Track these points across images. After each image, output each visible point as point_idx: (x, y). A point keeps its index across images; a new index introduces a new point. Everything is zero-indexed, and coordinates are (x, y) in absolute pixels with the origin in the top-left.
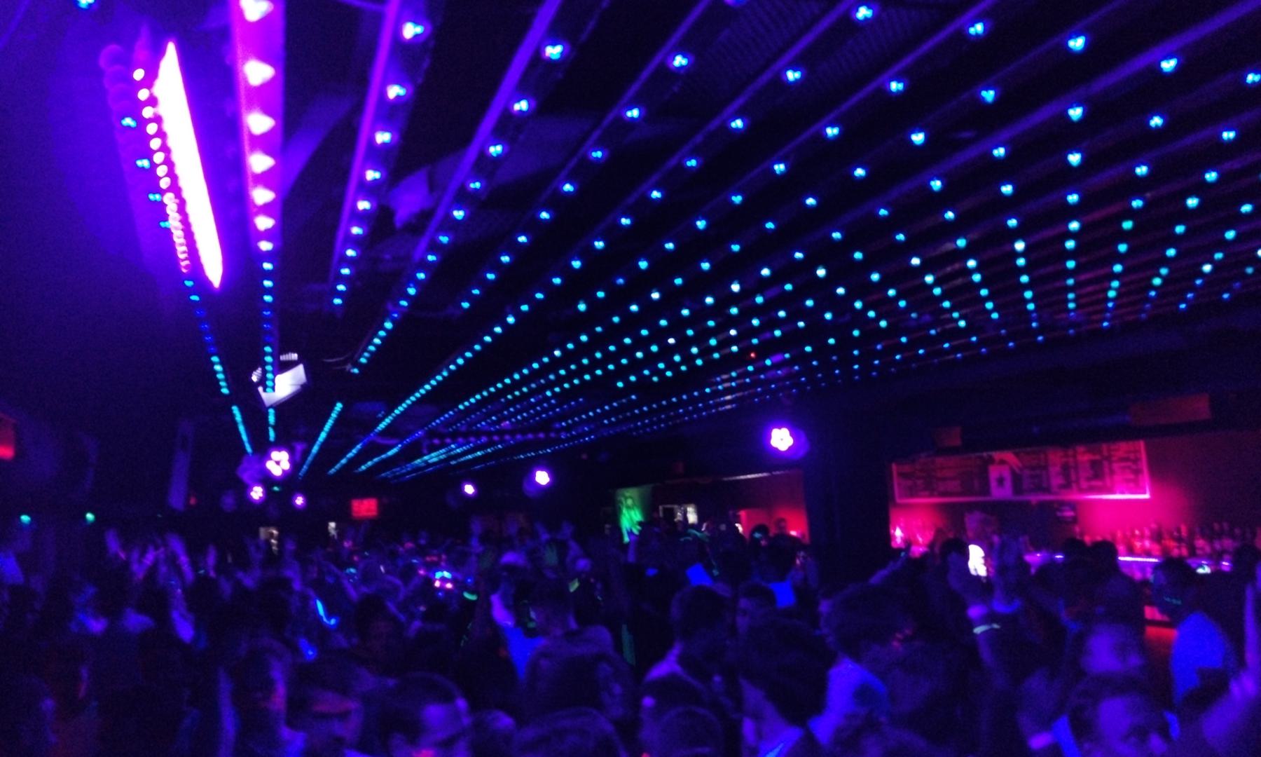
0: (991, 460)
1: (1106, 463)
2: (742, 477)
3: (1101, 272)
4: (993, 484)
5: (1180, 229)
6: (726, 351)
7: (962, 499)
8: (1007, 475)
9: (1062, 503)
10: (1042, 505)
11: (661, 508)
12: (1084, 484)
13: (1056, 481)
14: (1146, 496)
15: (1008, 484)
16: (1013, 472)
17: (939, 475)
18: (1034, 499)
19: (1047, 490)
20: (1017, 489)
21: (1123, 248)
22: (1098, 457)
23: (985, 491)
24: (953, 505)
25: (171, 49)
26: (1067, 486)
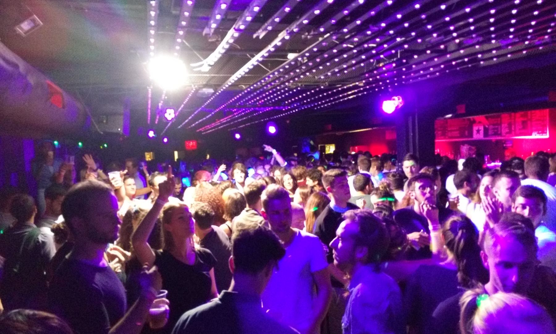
0: (473, 122)
1: (529, 122)
2: (351, 132)
3: (525, 25)
4: (475, 132)
5: (536, 13)
6: (341, 58)
7: (457, 140)
8: (482, 128)
9: (506, 141)
10: (497, 142)
11: (319, 146)
12: (518, 131)
13: (504, 131)
14: (547, 136)
15: (482, 132)
16: (485, 128)
17: (449, 129)
18: (493, 138)
19: (500, 135)
20: (486, 134)
21: (513, 21)
22: (525, 119)
23: (471, 135)
24: (456, 142)
25: (176, 160)
26: (510, 132)
